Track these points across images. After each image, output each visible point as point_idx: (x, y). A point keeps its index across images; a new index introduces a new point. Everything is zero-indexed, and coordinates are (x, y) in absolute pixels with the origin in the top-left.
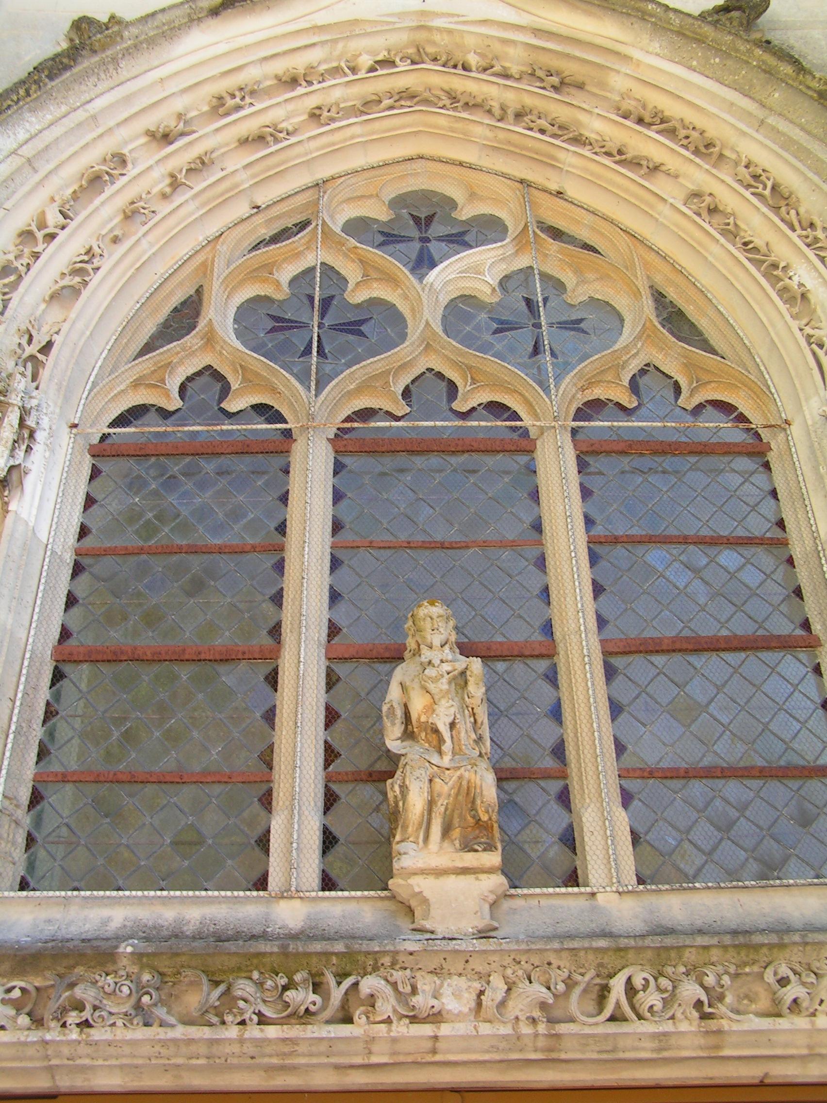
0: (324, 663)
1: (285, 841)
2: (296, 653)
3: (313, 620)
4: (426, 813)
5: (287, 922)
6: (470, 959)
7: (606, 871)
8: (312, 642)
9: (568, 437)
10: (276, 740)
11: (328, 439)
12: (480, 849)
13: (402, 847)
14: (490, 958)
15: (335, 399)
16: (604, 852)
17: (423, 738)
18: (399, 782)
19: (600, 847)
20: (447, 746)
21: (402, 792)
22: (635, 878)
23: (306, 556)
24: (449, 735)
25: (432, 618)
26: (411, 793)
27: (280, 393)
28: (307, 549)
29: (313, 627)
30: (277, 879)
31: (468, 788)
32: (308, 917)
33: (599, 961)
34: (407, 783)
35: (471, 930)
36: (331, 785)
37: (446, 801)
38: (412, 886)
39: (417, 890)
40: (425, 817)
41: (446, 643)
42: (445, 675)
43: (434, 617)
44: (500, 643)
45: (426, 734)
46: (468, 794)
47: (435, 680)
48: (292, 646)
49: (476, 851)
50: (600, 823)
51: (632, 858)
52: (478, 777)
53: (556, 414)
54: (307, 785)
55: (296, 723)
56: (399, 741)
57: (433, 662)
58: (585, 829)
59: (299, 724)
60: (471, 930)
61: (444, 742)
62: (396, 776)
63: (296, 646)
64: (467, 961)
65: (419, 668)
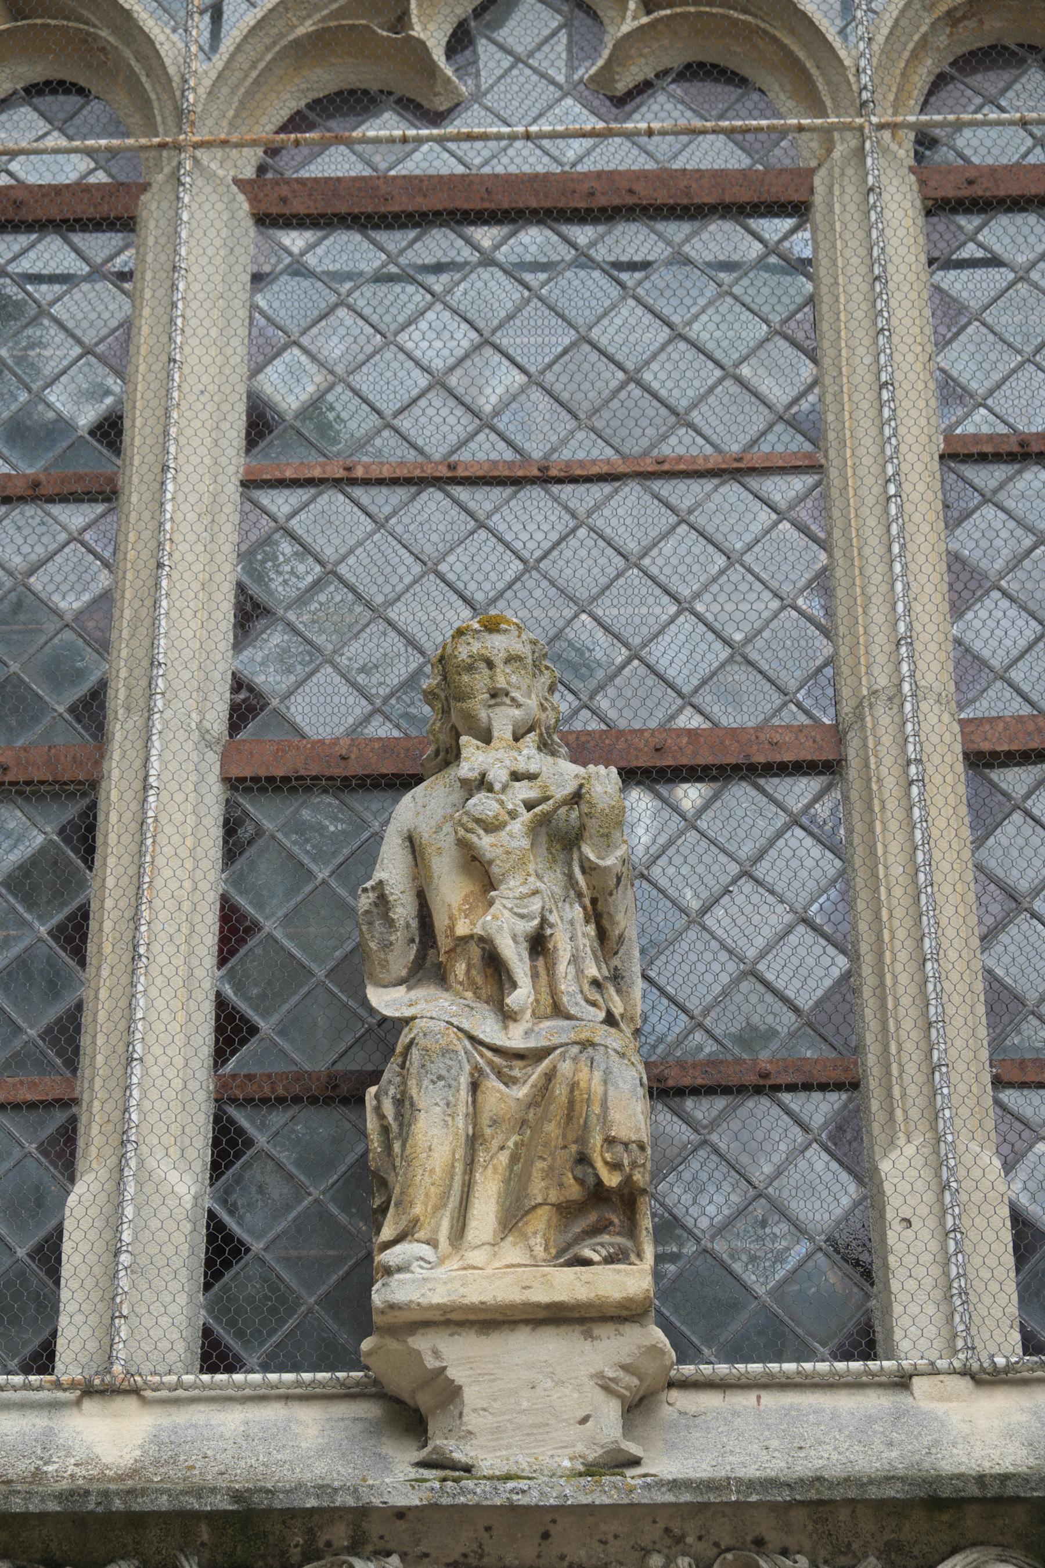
0: (214, 793)
1: (100, 1247)
2: (138, 764)
3: (186, 675)
4: (459, 1168)
5: (98, 1451)
6: (554, 1530)
7: (939, 1319)
8: (182, 735)
9: (904, 151)
10: (87, 994)
11: (236, 181)
12: (596, 1258)
13: (391, 1256)
14: (603, 1527)
15: (253, 66)
16: (936, 1271)
17: (461, 977)
18: (392, 1091)
19: (926, 1258)
20: (521, 996)
21: (399, 1115)
22: (1016, 1337)
23: (169, 507)
24: (527, 969)
25: (490, 665)
26: (422, 1117)
27: (103, 49)
28: (170, 487)
29: (184, 695)
30: (76, 1346)
31: (571, 1103)
32: (155, 1439)
33: (888, 1536)
34: (414, 1092)
35: (566, 1463)
36: (232, 1111)
37: (515, 1138)
38: (418, 1353)
39: (431, 1363)
40: (458, 1179)
41: (531, 729)
42: (522, 810)
43: (498, 661)
44: (689, 732)
45: (469, 967)
46: (569, 1118)
47: (491, 827)
48: (128, 745)
49: (587, 1262)
50: (930, 1197)
51: (1011, 1287)
52: (597, 1075)
53: (865, 95)
54: (160, 1105)
55: (135, 947)
56: (402, 989)
57: (490, 777)
58: (890, 1215)
59: (142, 950)
60: (566, 1463)
61: (514, 985)
62: (386, 1076)
63: (139, 744)
64: (546, 1536)
65: (457, 796)
